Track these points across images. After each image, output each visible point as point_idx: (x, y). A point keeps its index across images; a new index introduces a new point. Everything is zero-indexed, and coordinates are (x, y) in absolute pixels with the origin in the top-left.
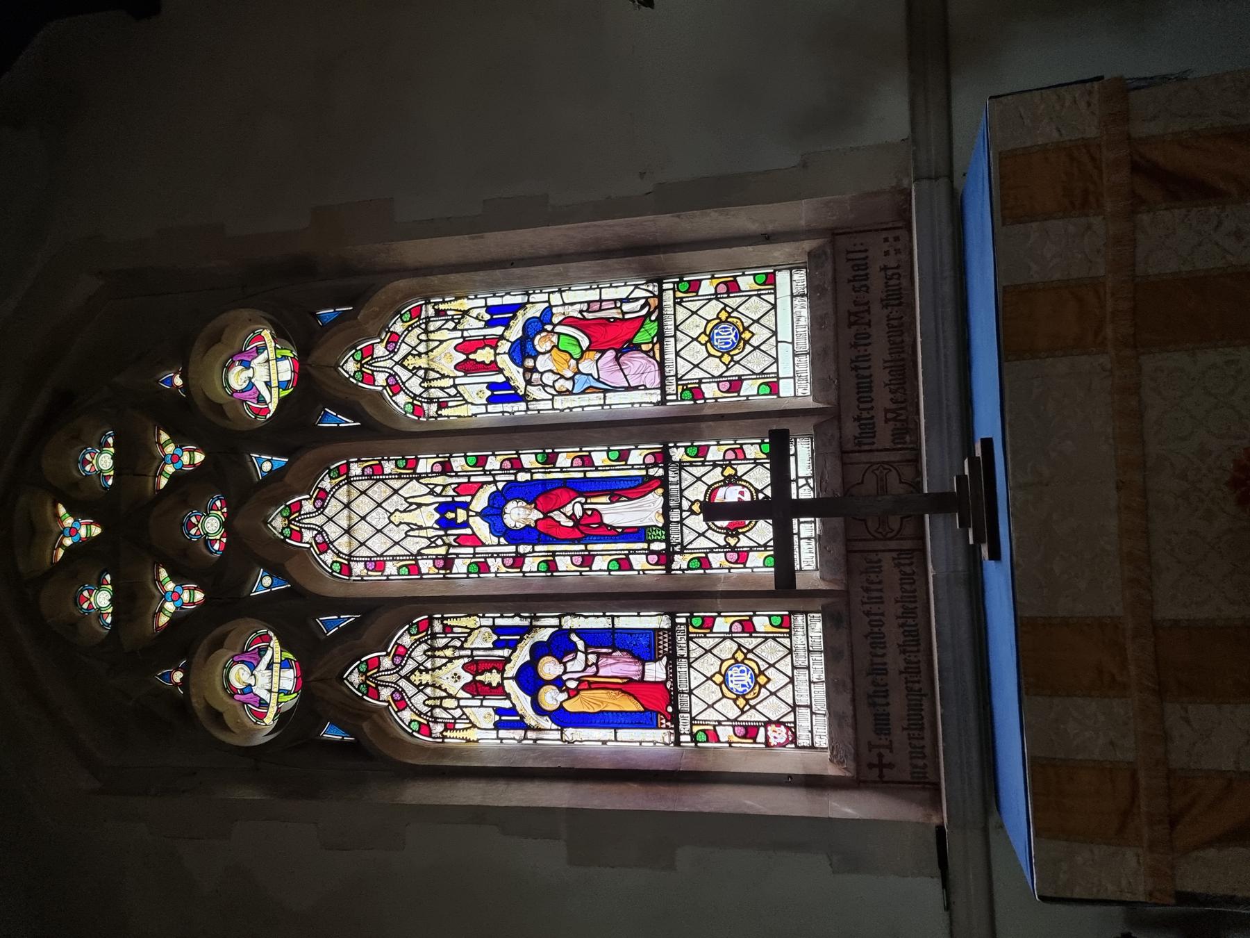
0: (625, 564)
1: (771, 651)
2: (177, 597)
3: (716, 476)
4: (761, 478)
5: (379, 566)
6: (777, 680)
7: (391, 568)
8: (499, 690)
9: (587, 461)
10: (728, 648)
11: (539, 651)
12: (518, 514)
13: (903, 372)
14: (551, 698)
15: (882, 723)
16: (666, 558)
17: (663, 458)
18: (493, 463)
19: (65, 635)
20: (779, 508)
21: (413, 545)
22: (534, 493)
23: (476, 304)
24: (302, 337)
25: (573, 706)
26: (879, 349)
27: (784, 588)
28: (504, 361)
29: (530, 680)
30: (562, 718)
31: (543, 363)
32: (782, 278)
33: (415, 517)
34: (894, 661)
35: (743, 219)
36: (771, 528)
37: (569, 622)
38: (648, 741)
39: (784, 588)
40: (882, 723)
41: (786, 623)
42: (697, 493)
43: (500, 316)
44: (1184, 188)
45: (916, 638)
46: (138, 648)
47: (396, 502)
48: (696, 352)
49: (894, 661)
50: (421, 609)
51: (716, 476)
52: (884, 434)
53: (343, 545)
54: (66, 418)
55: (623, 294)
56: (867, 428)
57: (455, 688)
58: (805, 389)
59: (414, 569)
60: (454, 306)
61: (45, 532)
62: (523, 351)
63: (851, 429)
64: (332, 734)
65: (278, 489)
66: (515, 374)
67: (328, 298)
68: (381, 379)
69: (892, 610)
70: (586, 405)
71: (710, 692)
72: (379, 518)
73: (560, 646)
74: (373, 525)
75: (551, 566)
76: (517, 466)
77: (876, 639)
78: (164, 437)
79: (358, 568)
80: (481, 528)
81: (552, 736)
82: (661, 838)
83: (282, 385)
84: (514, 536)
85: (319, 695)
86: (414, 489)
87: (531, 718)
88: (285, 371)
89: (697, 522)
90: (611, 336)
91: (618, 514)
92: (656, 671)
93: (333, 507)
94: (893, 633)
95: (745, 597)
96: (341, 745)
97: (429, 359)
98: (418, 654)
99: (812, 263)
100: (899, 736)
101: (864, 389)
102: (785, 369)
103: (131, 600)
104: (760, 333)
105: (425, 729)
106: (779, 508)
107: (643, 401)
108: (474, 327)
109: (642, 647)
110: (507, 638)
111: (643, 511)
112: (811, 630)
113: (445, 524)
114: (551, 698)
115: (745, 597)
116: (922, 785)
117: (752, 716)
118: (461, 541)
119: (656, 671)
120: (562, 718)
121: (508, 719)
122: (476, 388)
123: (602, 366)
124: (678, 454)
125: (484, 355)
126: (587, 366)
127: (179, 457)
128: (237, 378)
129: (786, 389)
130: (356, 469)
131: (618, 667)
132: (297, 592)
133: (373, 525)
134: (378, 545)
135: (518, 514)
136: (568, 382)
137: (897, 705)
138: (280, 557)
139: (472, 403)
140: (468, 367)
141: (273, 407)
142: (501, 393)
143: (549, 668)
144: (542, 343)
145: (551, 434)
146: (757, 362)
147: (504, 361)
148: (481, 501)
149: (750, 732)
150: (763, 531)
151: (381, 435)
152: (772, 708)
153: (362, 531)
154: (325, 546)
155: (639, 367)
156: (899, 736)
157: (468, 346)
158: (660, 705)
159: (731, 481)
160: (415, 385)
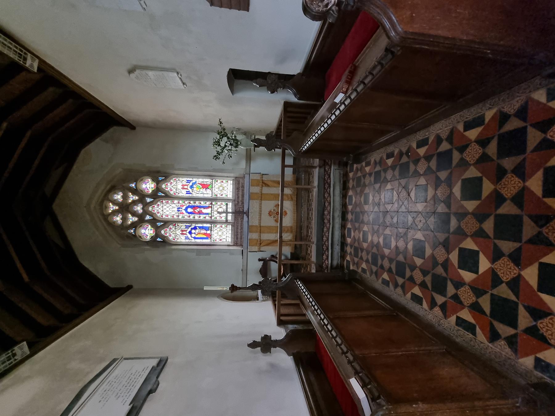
0: (205, 218)
1: (224, 230)
2: (132, 219)
3: (219, 207)
4: (225, 207)
5: (167, 216)
6: (225, 233)
7: (169, 217)
8: (186, 234)
9: (200, 203)
10: (219, 229)
11: (192, 229)
12: (190, 210)
13: (243, 196)
14: (193, 235)
15: (237, 238)
16: (211, 217)
17: (212, 204)
18: (186, 202)
19: (112, 225)
20: (227, 212)
21: (173, 213)
22: (194, 207)
23: (185, 179)
24: (158, 182)
25: (197, 236)
26: (240, 193)
27: (226, 222)
28: (189, 188)
29: (190, 233)
30: (195, 238)
31: (194, 189)
32: (229, 181)
33: (174, 209)
34: (239, 231)
35: (225, 175)
36: (284, 335)
37: (197, 225)
38: (207, 241)
39: (226, 222)
40: (237, 238)
41: (226, 226)
42: (216, 209)
43: (188, 182)
44: (267, 185)
45: (242, 228)
46: (124, 227)
47: (171, 207)
48: (217, 190)
49: (239, 231)
50: (174, 222)
51: (219, 207)
52: (240, 203)
53: (161, 213)
54: (113, 189)
55: (207, 181)
56: (238, 202)
57: (179, 234)
58: (231, 196)
59: (173, 217)
60: (181, 179)
61: (107, 207)
62: (192, 187)
63: (236, 202)
64: (159, 239)
65: (151, 203)
66: (191, 191)
67: (160, 175)
68: (169, 189)
69: (239, 225)
70: (201, 196)
71: (216, 235)
72: (168, 209)
73: (195, 228)
74: (165, 210)
75: (194, 217)
76: (190, 203)
77: (237, 228)
78: (130, 194)
79: (164, 216)
80: (184, 212)
81: (193, 240)
82: (208, 252)
83: (152, 188)
84: (189, 213)
85: (157, 235)
86: (173, 205)
87: (190, 238)
88: (153, 186)
89: (216, 213)
90: (205, 186)
91: (204, 211)
92: (209, 232)
93: (160, 207)
94: (239, 228)
95: (221, 223)
96: (160, 243)
97: (176, 186)
98: (173, 229)
99: (233, 180)
100: (239, 240)
101: (238, 197)
102: (229, 193)
103: (124, 219)
104: (225, 188)
105: (174, 239)
106: (227, 212)
107: (209, 196)
108: (184, 183)
109: (207, 229)
110: (187, 227)
111: (208, 211)
112: (230, 227)
113: (178, 211)
114: (193, 235)
115: (221, 223)
116: (241, 245)
117: (221, 238)
118: (181, 213)
119: (209, 232)
120: (195, 238)
121: (187, 238)
122: (184, 192)
123: (203, 190)
124: (213, 203)
125: (186, 187)
126: (201, 190)
127: (132, 198)
128: (144, 186)
129: (229, 196)
130: (164, 202)
131: (203, 231)
132: (154, 219)
133: (165, 210)
134: (167, 213)
135: (190, 210)
136: (198, 192)
137: (239, 236)
138: (151, 214)
139: (183, 193)
140: (183, 188)
141: (150, 192)
142: (188, 193)
143: (193, 231)
144: (194, 186)
145: (195, 199)
146: (225, 192)
147: (189, 188)
148: (184, 208)
149: (221, 240)
150: (224, 215)
151: (167, 196)
152: (224, 237)
153: (165, 211)
154: (158, 213)
155: (209, 191)
156: (239, 240)
157: (183, 185)
158: (209, 236)
159: (221, 207)
160: (174, 190)
